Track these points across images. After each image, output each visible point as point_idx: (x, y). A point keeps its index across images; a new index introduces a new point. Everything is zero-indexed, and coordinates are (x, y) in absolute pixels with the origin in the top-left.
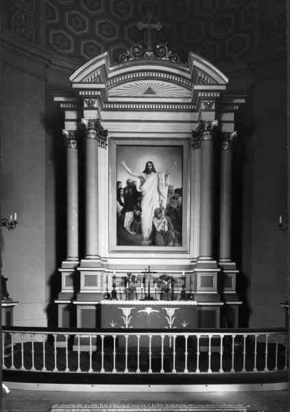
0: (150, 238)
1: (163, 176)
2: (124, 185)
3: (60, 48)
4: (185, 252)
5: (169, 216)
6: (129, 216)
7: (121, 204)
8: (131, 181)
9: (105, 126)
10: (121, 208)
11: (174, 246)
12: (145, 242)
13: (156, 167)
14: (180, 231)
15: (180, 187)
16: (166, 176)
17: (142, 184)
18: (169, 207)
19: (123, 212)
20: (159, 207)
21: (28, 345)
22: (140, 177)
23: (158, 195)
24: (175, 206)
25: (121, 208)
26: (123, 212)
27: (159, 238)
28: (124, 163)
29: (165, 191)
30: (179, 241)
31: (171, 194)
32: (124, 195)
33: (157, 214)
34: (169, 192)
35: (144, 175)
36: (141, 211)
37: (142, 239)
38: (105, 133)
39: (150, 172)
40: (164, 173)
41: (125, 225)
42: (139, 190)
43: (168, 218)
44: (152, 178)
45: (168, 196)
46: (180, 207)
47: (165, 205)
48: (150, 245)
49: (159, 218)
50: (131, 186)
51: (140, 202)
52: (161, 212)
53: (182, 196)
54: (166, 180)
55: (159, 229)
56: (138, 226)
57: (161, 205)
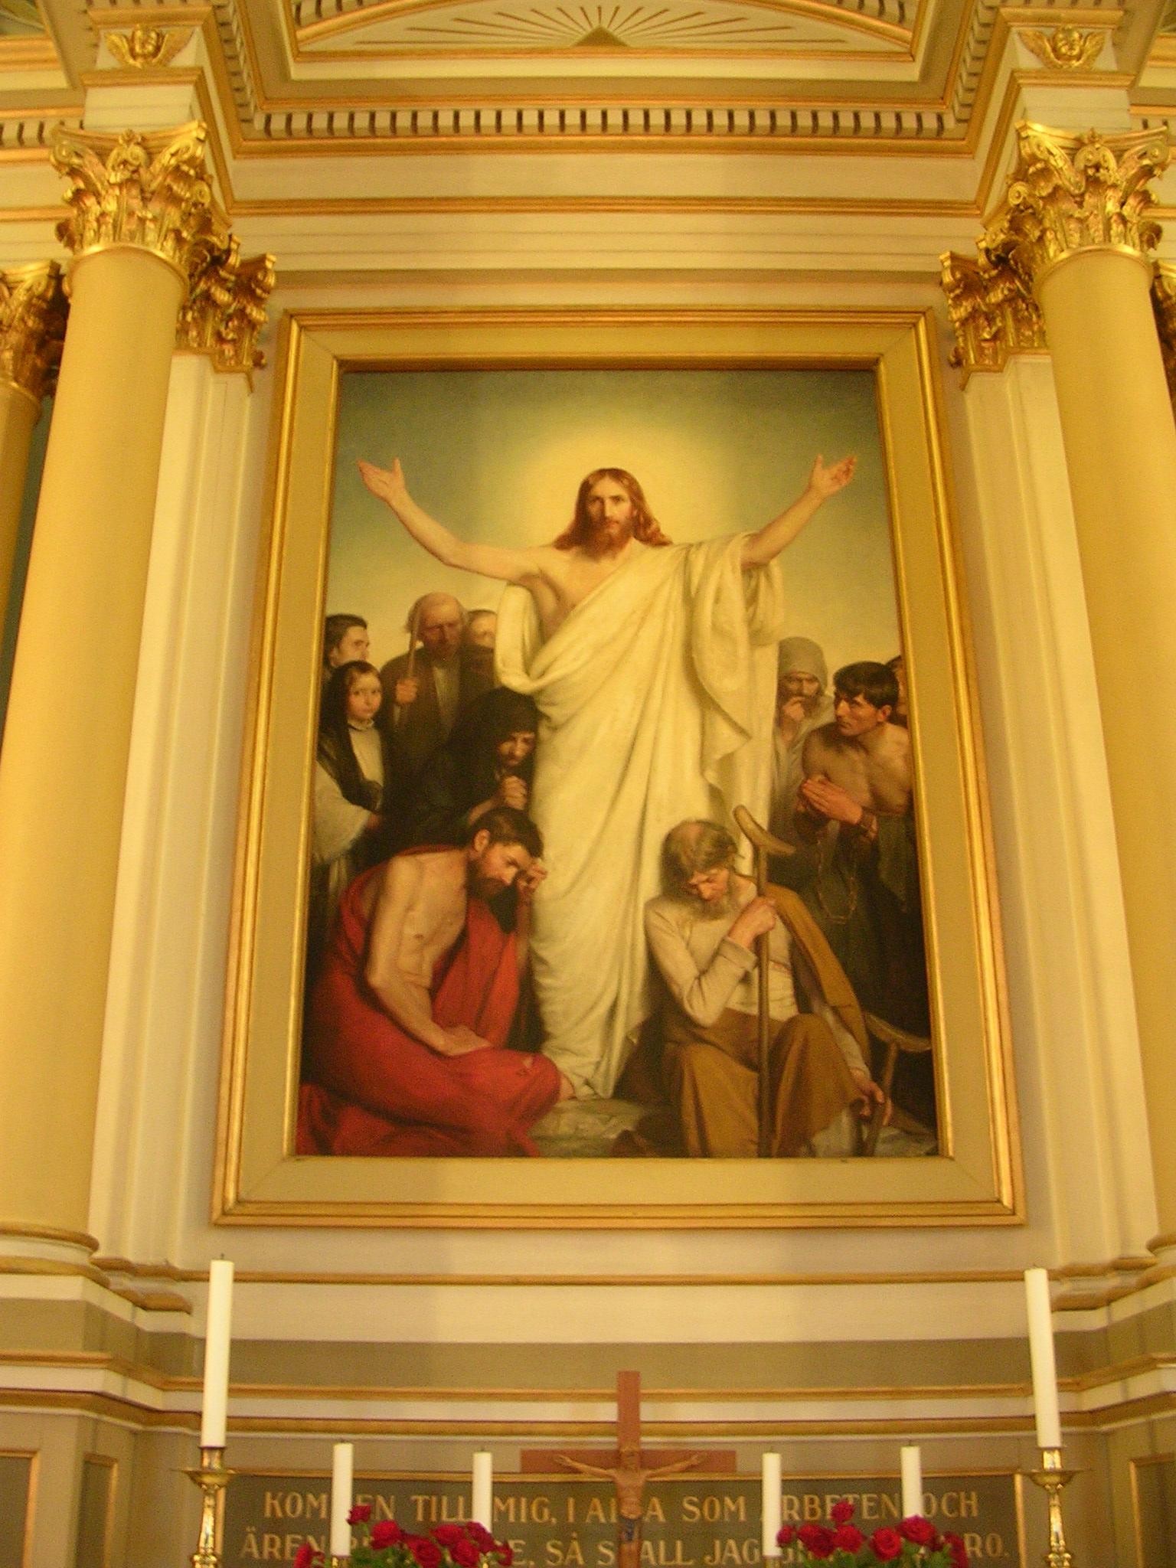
0: (623, 1089)
1: (724, 578)
2: (386, 641)
3: (819, 692)
4: (983, 1215)
5: (797, 887)
6: (420, 894)
7: (353, 788)
8: (445, 612)
9: (247, 238)
10: (353, 820)
11: (862, 1149)
12: (563, 1122)
13: (656, 506)
14: (917, 1015)
15: (882, 655)
16: (752, 569)
17: (544, 631)
18: (797, 815)
19: (372, 855)
20: (699, 808)
21: (1060, 1306)
22: (525, 580)
23: (689, 716)
24: (846, 803)
25: (353, 820)
26: (372, 855)
27: (718, 1083)
28: (391, 484)
29: (748, 685)
30: (907, 1100)
31: (811, 704)
32: (382, 720)
33: (683, 870)
34: (784, 695)
35: (562, 566)
36: (534, 845)
37: (545, 1096)
38: (249, 282)
39: (613, 546)
40: (738, 550)
41: (380, 976)
42: (513, 677)
43: (791, 901)
44: (626, 591)
45: (781, 720)
46: (901, 817)
47: (754, 797)
48: (625, 1147)
49: (708, 909)
50: (450, 646)
51: (527, 770)
52: (723, 850)
53: (902, 721)
54: (752, 599)
55: (707, 1004)
56: (506, 988)
57: (716, 795)
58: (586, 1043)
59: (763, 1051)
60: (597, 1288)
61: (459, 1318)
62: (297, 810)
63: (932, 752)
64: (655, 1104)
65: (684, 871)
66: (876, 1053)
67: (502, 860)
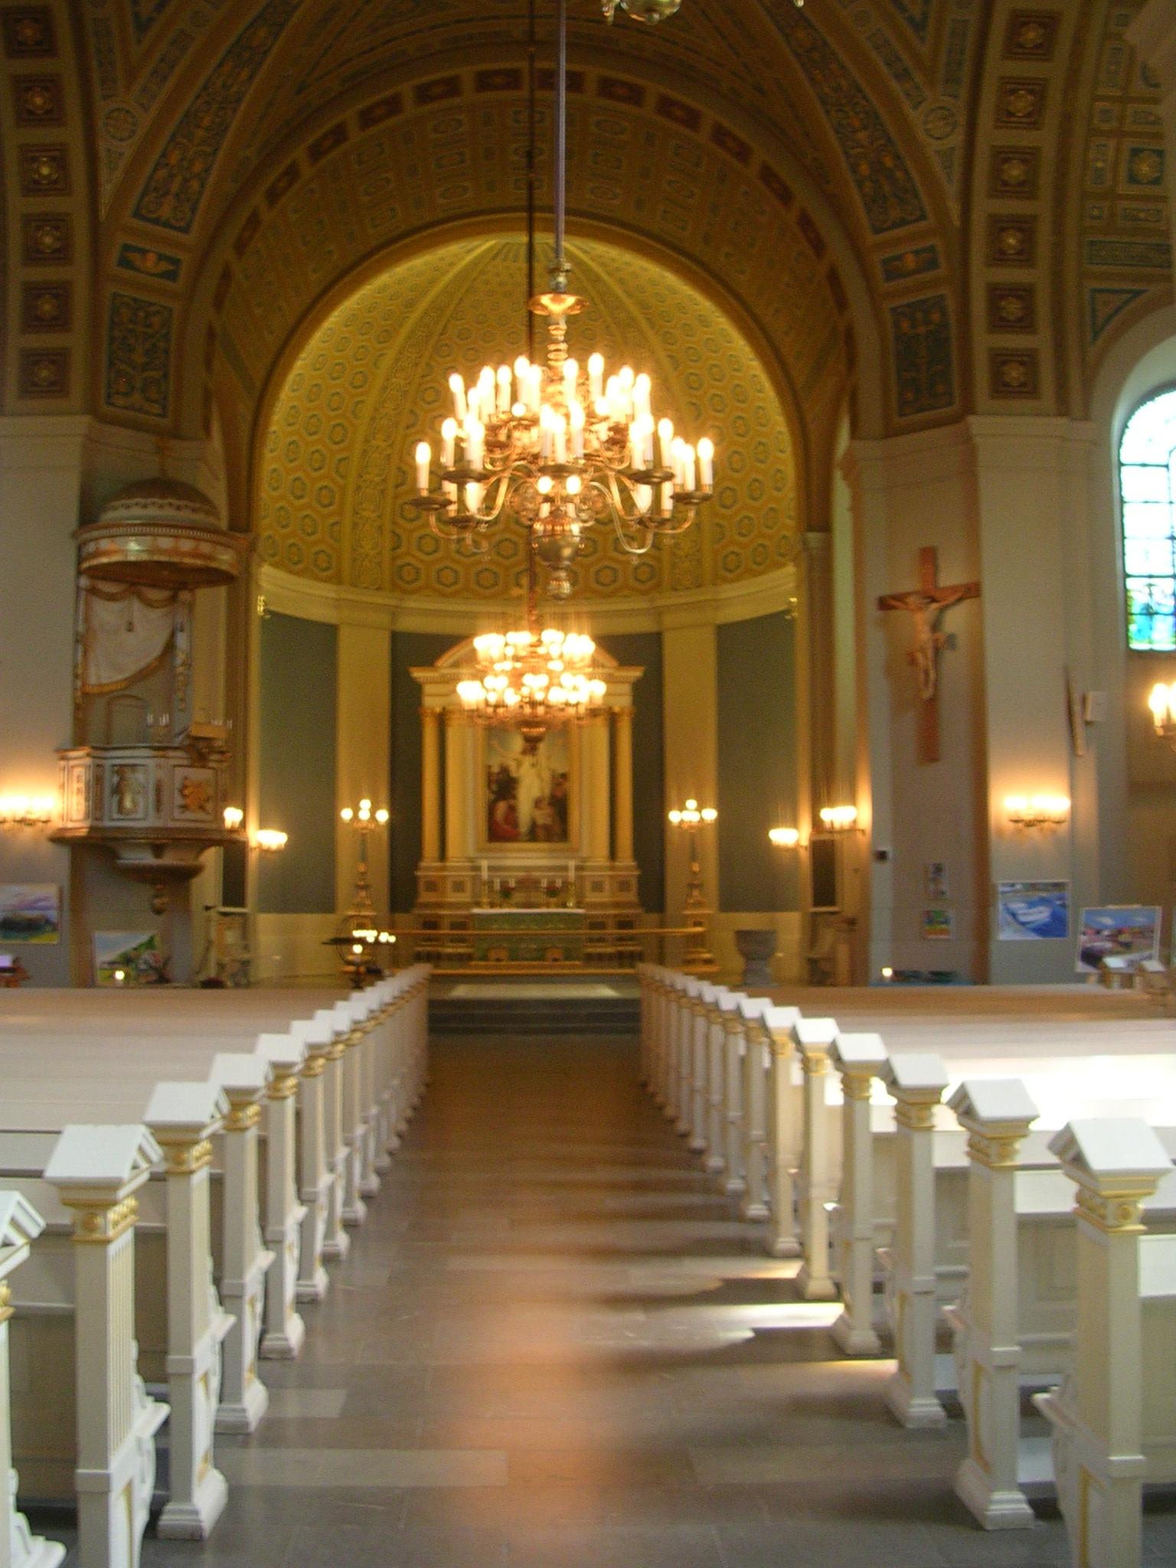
2: (496, 769)
27: (541, 833)
47: (547, 792)
50: (505, 770)
58: (524, 825)
59: (546, 828)
60: (526, 858)
61: (509, 863)
63: (574, 788)
64: (533, 835)
65: (538, 803)
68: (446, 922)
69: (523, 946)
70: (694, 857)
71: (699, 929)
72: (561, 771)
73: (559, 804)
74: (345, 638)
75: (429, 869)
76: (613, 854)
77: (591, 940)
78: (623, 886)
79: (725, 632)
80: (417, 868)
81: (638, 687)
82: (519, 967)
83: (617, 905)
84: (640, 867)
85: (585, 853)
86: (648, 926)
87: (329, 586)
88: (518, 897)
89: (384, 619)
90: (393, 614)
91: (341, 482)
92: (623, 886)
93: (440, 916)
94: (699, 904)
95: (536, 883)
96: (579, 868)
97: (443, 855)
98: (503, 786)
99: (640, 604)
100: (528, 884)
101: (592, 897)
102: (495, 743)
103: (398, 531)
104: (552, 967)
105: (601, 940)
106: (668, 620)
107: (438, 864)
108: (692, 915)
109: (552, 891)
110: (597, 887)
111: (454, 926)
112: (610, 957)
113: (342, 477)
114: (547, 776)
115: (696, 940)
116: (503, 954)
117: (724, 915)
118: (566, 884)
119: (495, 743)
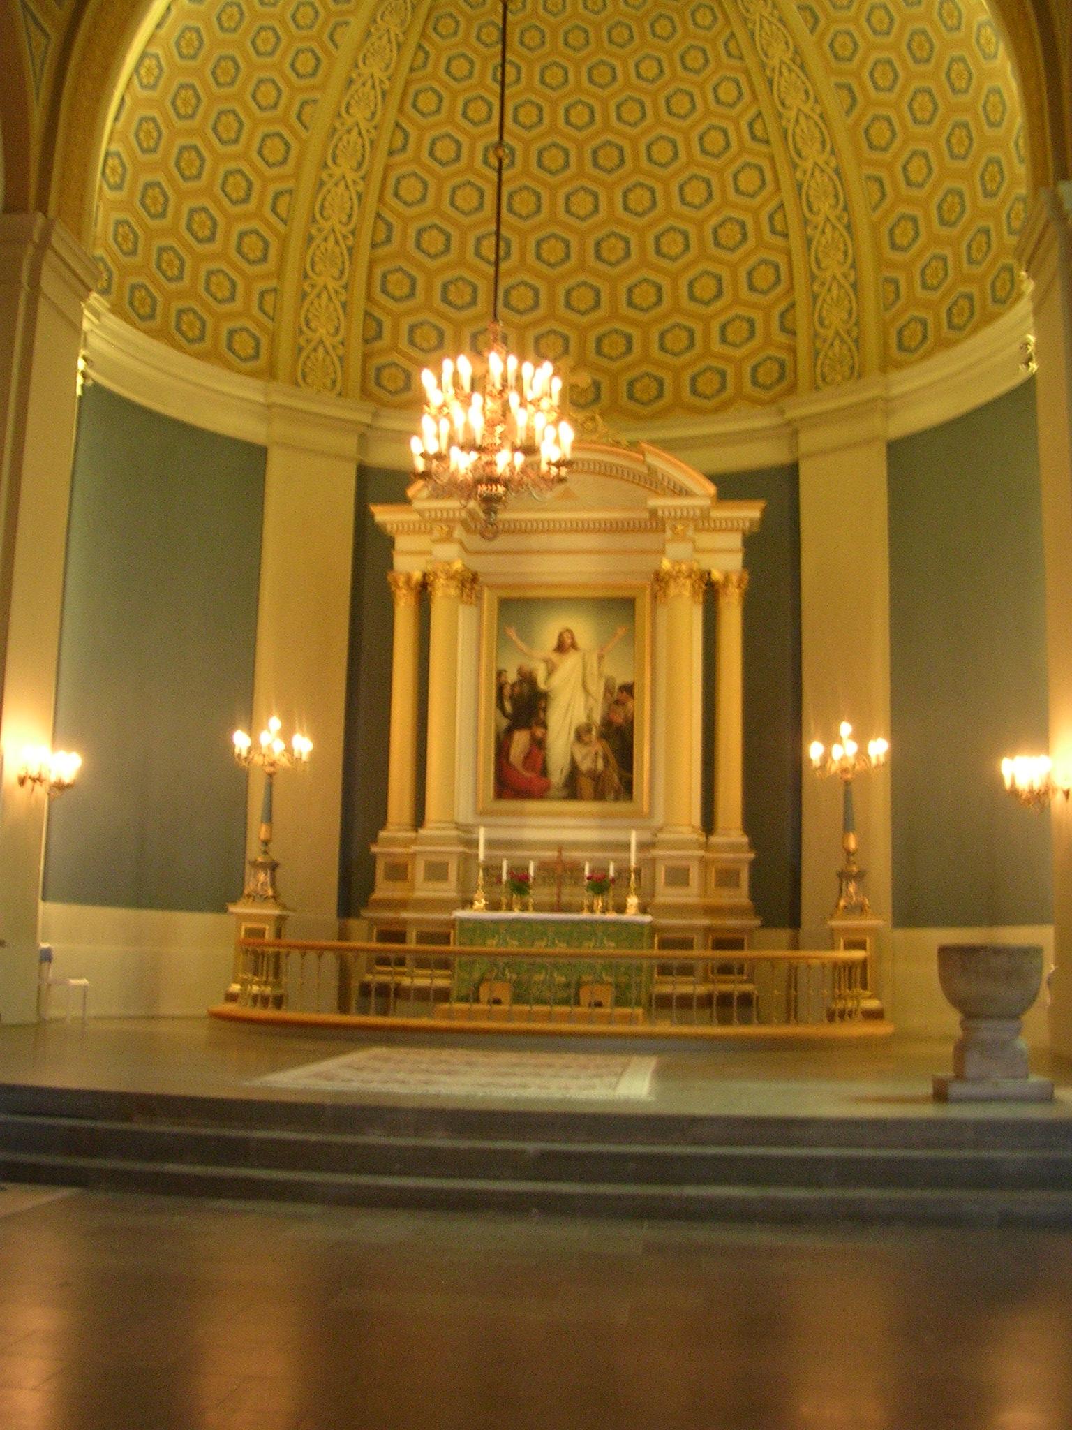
2: (512, 677)
11: (617, 799)
19: (510, 731)
26: (510, 731)
27: (586, 785)
46: (630, 723)
50: (527, 679)
58: (557, 776)
59: (596, 777)
60: (559, 828)
61: (529, 835)
62: (489, 720)
63: (642, 708)
64: (572, 789)
65: (581, 735)
66: (621, 779)
67: (539, 732)
68: (412, 934)
69: (539, 977)
70: (848, 825)
71: (858, 954)
72: (620, 680)
73: (618, 737)
74: (277, 465)
75: (392, 842)
76: (709, 822)
77: (665, 970)
78: (727, 878)
79: (901, 453)
80: (375, 840)
81: (754, 545)
82: (529, 1017)
83: (709, 911)
84: (753, 845)
85: (659, 820)
86: (771, 947)
87: (259, 384)
88: (538, 894)
89: (349, 444)
90: (362, 436)
91: (282, 228)
92: (727, 878)
93: (404, 922)
94: (860, 909)
95: (576, 868)
96: (642, 846)
97: (419, 819)
98: (524, 706)
99: (763, 420)
100: (560, 871)
101: (666, 895)
102: (512, 633)
103: (378, 313)
104: (588, 1019)
105: (686, 970)
106: (807, 441)
107: (412, 835)
108: (846, 930)
109: (600, 884)
110: (678, 877)
111: (423, 938)
112: (706, 1001)
113: (285, 222)
114: (598, 689)
115: (854, 975)
116: (504, 992)
117: (901, 934)
118: (623, 872)
119: (512, 633)
